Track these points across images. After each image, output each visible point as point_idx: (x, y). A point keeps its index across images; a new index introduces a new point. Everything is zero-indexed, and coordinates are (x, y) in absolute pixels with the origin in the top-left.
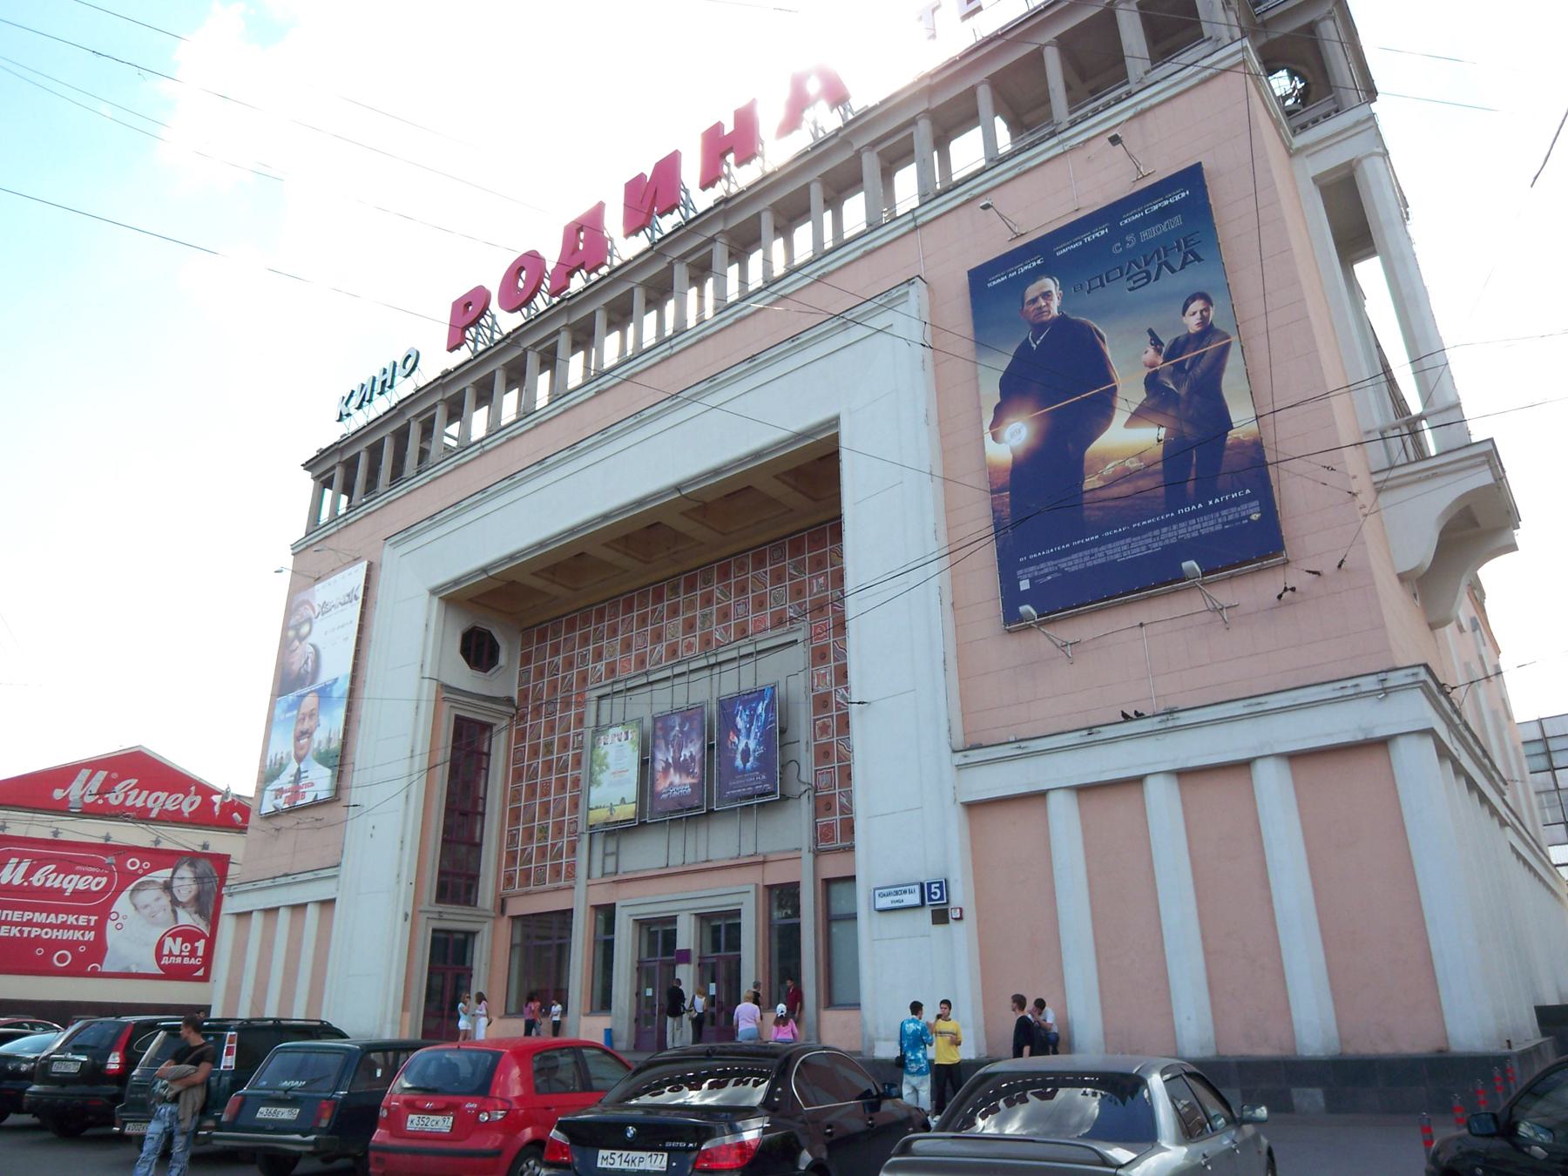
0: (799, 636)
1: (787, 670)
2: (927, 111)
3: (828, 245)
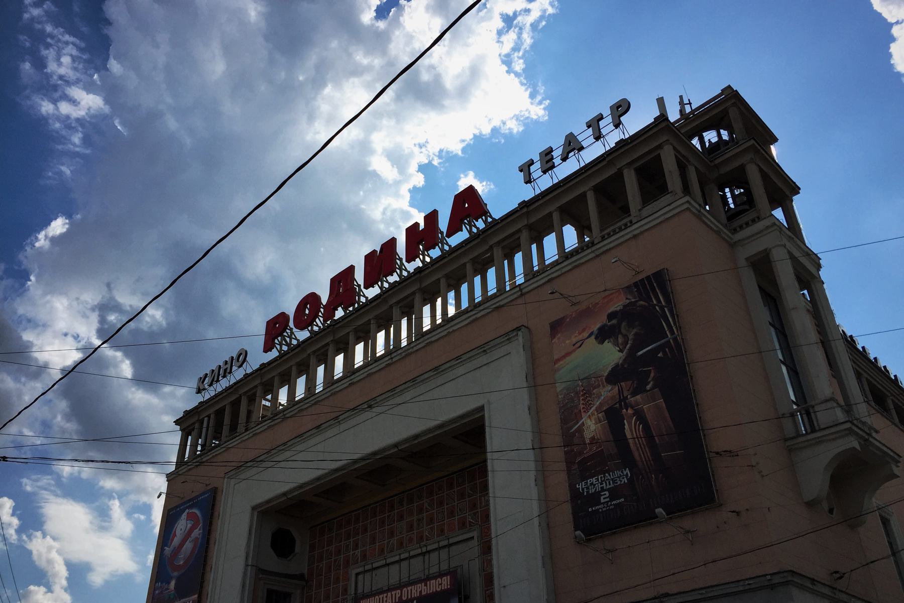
0: (475, 534)
1: (465, 556)
2: (526, 225)
3: (439, 321)
